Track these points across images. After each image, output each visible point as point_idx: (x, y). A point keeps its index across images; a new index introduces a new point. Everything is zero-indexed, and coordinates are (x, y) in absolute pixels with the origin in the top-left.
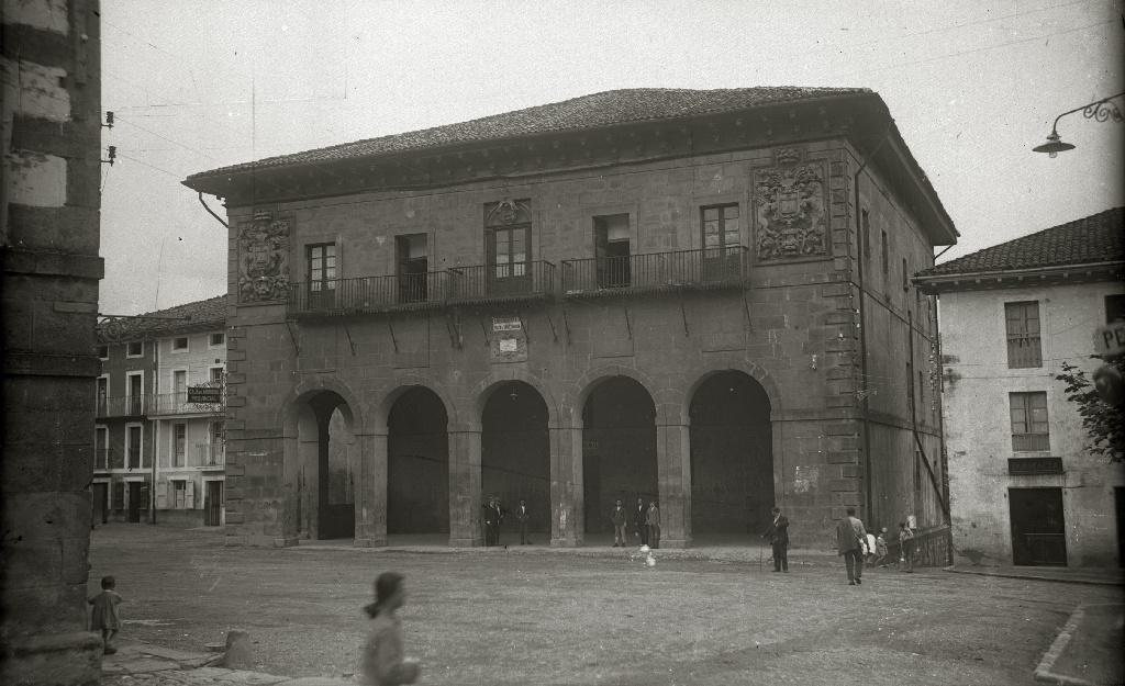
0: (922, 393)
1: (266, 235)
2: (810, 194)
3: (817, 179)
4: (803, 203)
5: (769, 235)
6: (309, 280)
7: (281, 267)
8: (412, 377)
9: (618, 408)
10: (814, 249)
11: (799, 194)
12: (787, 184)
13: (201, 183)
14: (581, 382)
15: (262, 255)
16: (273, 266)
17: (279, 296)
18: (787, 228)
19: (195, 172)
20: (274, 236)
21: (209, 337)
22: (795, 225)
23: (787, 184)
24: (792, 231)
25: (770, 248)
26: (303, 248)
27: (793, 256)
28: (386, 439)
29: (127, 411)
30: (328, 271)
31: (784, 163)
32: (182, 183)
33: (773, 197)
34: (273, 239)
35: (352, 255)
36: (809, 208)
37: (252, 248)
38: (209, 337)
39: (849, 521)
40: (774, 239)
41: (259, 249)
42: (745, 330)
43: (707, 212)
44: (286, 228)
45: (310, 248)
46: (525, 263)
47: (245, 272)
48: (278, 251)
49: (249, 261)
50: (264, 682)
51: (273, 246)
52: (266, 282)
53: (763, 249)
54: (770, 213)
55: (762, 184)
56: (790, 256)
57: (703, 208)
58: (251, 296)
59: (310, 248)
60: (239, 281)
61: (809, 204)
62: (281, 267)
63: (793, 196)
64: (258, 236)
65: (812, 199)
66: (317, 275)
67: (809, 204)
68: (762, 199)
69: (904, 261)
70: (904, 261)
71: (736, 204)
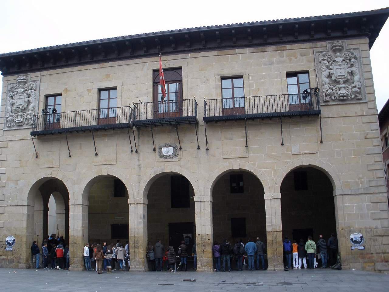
0: (302, 281)
1: (23, 90)
2: (352, 65)
5: (330, 88)
7: (30, 107)
9: (237, 187)
10: (356, 96)
11: (345, 66)
14: (149, 174)
16: (25, 106)
17: (27, 124)
18: (340, 84)
20: (28, 91)
22: (344, 83)
24: (343, 85)
25: (330, 95)
26: (43, 96)
27: (343, 100)
28: (43, 212)
31: (336, 49)
33: (331, 67)
36: (352, 74)
37: (16, 97)
40: (333, 90)
41: (18, 97)
44: (35, 86)
45: (47, 97)
47: (10, 111)
48: (29, 99)
49: (12, 105)
51: (27, 96)
52: (22, 116)
54: (330, 76)
55: (324, 60)
58: (12, 124)
60: (5, 115)
63: (342, 67)
64: (18, 90)
65: (353, 69)
68: (324, 68)
71: (307, 72)
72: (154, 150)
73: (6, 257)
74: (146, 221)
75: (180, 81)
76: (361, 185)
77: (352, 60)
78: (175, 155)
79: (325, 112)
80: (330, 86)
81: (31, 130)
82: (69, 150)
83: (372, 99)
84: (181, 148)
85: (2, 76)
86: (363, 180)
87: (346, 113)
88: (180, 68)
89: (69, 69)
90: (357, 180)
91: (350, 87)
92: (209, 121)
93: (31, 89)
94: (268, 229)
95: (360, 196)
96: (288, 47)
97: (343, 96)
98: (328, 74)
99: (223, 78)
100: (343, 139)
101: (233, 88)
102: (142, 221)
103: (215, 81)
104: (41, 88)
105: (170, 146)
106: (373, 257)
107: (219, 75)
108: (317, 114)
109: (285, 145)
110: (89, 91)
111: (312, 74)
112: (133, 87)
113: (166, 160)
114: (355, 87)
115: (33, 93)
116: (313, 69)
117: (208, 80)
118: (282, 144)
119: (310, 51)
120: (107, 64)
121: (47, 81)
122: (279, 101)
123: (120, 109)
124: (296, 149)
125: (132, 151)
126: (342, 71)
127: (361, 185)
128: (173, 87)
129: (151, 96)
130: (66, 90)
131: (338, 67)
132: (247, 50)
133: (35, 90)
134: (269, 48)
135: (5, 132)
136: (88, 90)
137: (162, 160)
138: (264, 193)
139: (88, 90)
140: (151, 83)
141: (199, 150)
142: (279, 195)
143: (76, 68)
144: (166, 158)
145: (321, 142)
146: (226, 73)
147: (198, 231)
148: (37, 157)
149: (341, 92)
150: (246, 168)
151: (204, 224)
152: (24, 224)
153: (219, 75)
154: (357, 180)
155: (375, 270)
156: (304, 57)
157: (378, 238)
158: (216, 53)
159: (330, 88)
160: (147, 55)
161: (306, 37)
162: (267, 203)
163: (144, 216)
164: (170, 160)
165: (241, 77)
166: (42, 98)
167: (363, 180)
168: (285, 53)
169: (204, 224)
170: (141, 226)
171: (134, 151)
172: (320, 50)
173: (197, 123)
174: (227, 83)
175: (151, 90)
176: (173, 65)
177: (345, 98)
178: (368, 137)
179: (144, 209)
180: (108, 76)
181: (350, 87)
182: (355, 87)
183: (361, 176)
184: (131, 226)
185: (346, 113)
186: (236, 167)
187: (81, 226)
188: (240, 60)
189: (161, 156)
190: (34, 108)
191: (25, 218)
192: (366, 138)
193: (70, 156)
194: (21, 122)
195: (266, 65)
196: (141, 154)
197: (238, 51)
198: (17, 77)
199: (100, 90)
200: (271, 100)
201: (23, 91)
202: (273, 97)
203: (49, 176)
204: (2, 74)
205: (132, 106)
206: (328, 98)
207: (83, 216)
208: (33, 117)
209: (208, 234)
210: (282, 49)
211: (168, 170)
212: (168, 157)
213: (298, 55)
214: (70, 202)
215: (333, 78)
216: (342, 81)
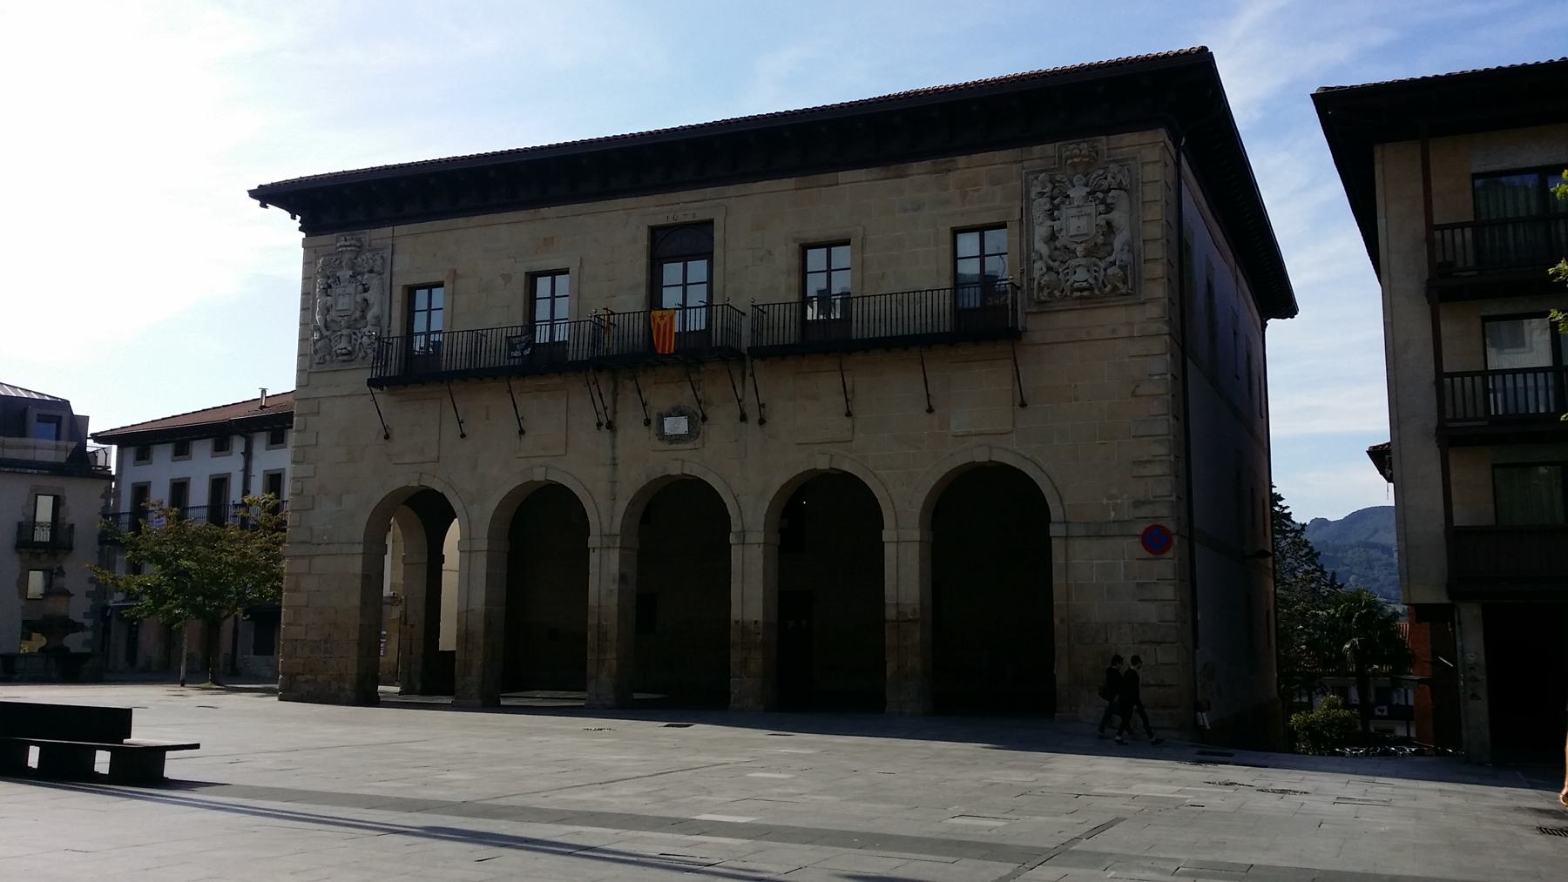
4: (1101, 220)
5: (1049, 269)
8: (679, 463)
11: (1091, 209)
12: (1077, 193)
14: (633, 479)
16: (358, 314)
19: (266, 181)
23: (1077, 193)
27: (1089, 297)
29: (746, 342)
30: (436, 318)
32: (253, 194)
36: (1110, 228)
43: (962, 238)
45: (411, 291)
50: (1322, 855)
53: (1041, 288)
56: (1080, 298)
57: (956, 232)
61: (1109, 224)
62: (369, 316)
67: (1109, 224)
69: (197, 746)
70: (197, 746)
75: (708, 255)
78: (693, 434)
79: (1039, 328)
84: (704, 419)
87: (1114, 331)
89: (460, 221)
90: (1105, 501)
91: (1102, 265)
93: (371, 271)
96: (962, 160)
97: (1081, 290)
100: (1077, 399)
105: (681, 414)
107: (795, 240)
109: (937, 411)
110: (507, 278)
113: (673, 446)
114: (1113, 263)
115: (374, 282)
116: (1017, 217)
117: (770, 253)
118: (930, 410)
120: (545, 211)
126: (1083, 222)
128: (698, 269)
130: (455, 275)
136: (503, 276)
138: (880, 526)
139: (503, 276)
140: (643, 261)
144: (671, 442)
146: (812, 235)
148: (387, 437)
150: (846, 467)
151: (749, 594)
152: (355, 600)
153: (795, 240)
154: (1105, 501)
157: (1145, 647)
158: (789, 183)
160: (637, 189)
161: (449, 700)
164: (680, 446)
168: (952, 177)
169: (749, 594)
181: (1102, 265)
182: (1113, 263)
183: (1114, 491)
186: (822, 464)
190: (378, 319)
191: (358, 582)
193: (463, 436)
197: (843, 176)
206: (1044, 296)
212: (676, 439)
213: (988, 178)
216: (1080, 249)
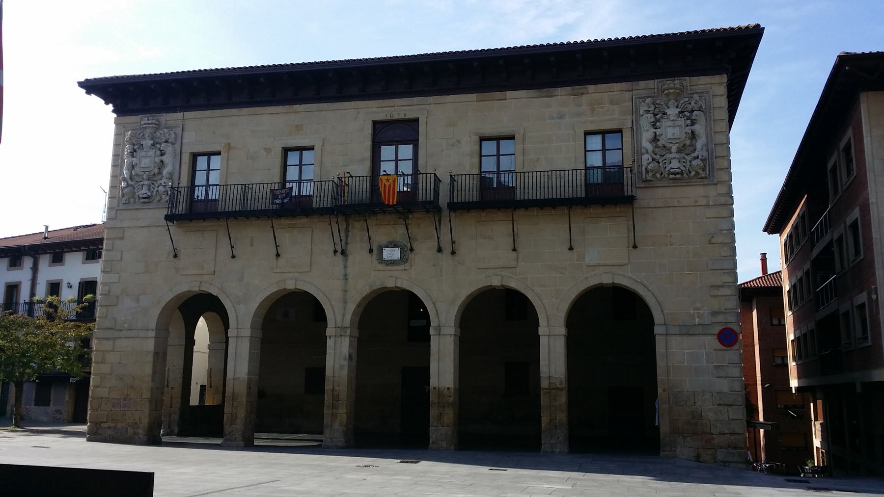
2: (693, 124)
3: (700, 109)
5: (653, 160)
6: (192, 186)
11: (682, 122)
12: (672, 112)
13: (91, 86)
15: (147, 160)
16: (156, 171)
21: (67, 393)
27: (679, 178)
34: (158, 146)
35: (242, 151)
38: (67, 393)
39: (797, 389)
42: (439, 327)
45: (195, 156)
46: (411, 175)
48: (162, 158)
59: (195, 156)
63: (677, 123)
66: (200, 178)
71: (620, 131)
72: (371, 251)
73: (113, 425)
74: (354, 363)
75: (415, 142)
76: (697, 320)
77: (695, 113)
78: (404, 260)
79: (644, 197)
80: (655, 156)
81: (165, 212)
82: (232, 247)
83: (726, 178)
84: (412, 250)
85: (115, 116)
86: (701, 312)
88: (417, 120)
89: (234, 111)
90: (692, 312)
92: (454, 207)
93: (166, 142)
94: (544, 384)
95: (696, 338)
96: (591, 88)
97: (675, 174)
98: (653, 136)
99: (483, 139)
100: (671, 244)
101: (498, 155)
102: (346, 363)
103: (469, 145)
104: (184, 141)
105: (395, 246)
106: (713, 438)
107: (476, 134)
108: (630, 200)
109: (575, 249)
110: (268, 150)
111: (627, 136)
112: (336, 143)
113: (389, 268)
114: (697, 157)
115: (169, 149)
116: (630, 126)
118: (571, 249)
119: (628, 95)
120: (297, 107)
121: (197, 128)
122: (566, 179)
123: (309, 178)
124: (592, 256)
125: (335, 252)
127: (697, 320)
128: (406, 151)
129: (368, 164)
130: (229, 147)
131: (670, 123)
132: (522, 93)
133: (173, 144)
134: (560, 91)
135: (119, 212)
136: (265, 149)
137: (382, 267)
139: (265, 149)
140: (368, 143)
141: (440, 254)
142: (563, 331)
143: (246, 110)
144: (388, 265)
145: (635, 247)
147: (434, 382)
148: (175, 256)
149: (671, 166)
151: (443, 369)
152: (148, 370)
153: (476, 134)
154: (692, 312)
155: (715, 462)
156: (616, 107)
157: (721, 408)
158: (473, 97)
159: (653, 160)
162: (543, 341)
163: (350, 357)
165: (512, 138)
166: (186, 159)
167: (701, 312)
168: (585, 98)
169: (443, 369)
170: (345, 372)
171: (340, 250)
172: (643, 93)
173: (438, 210)
174: (489, 148)
175: (368, 154)
176: (405, 115)
177: (678, 176)
178: (713, 241)
179: (350, 345)
180: (299, 128)
181: (688, 158)
182: (697, 157)
183: (698, 305)
184: (328, 372)
185: (679, 202)
187: (246, 370)
188: (514, 109)
189: (381, 260)
191: (150, 358)
192: (710, 242)
193: (233, 257)
194: (149, 197)
195: (553, 118)
196: (350, 258)
198: (141, 120)
199: (286, 151)
200: (554, 177)
201: (153, 145)
202: (562, 172)
203: (196, 289)
204: (114, 111)
205: (336, 180)
206: (649, 177)
207: (251, 355)
208: (169, 190)
209: (448, 389)
210: (581, 91)
211: (390, 284)
212: (393, 263)
213: (608, 103)
214: (230, 333)
215: (660, 144)
216: (674, 148)
